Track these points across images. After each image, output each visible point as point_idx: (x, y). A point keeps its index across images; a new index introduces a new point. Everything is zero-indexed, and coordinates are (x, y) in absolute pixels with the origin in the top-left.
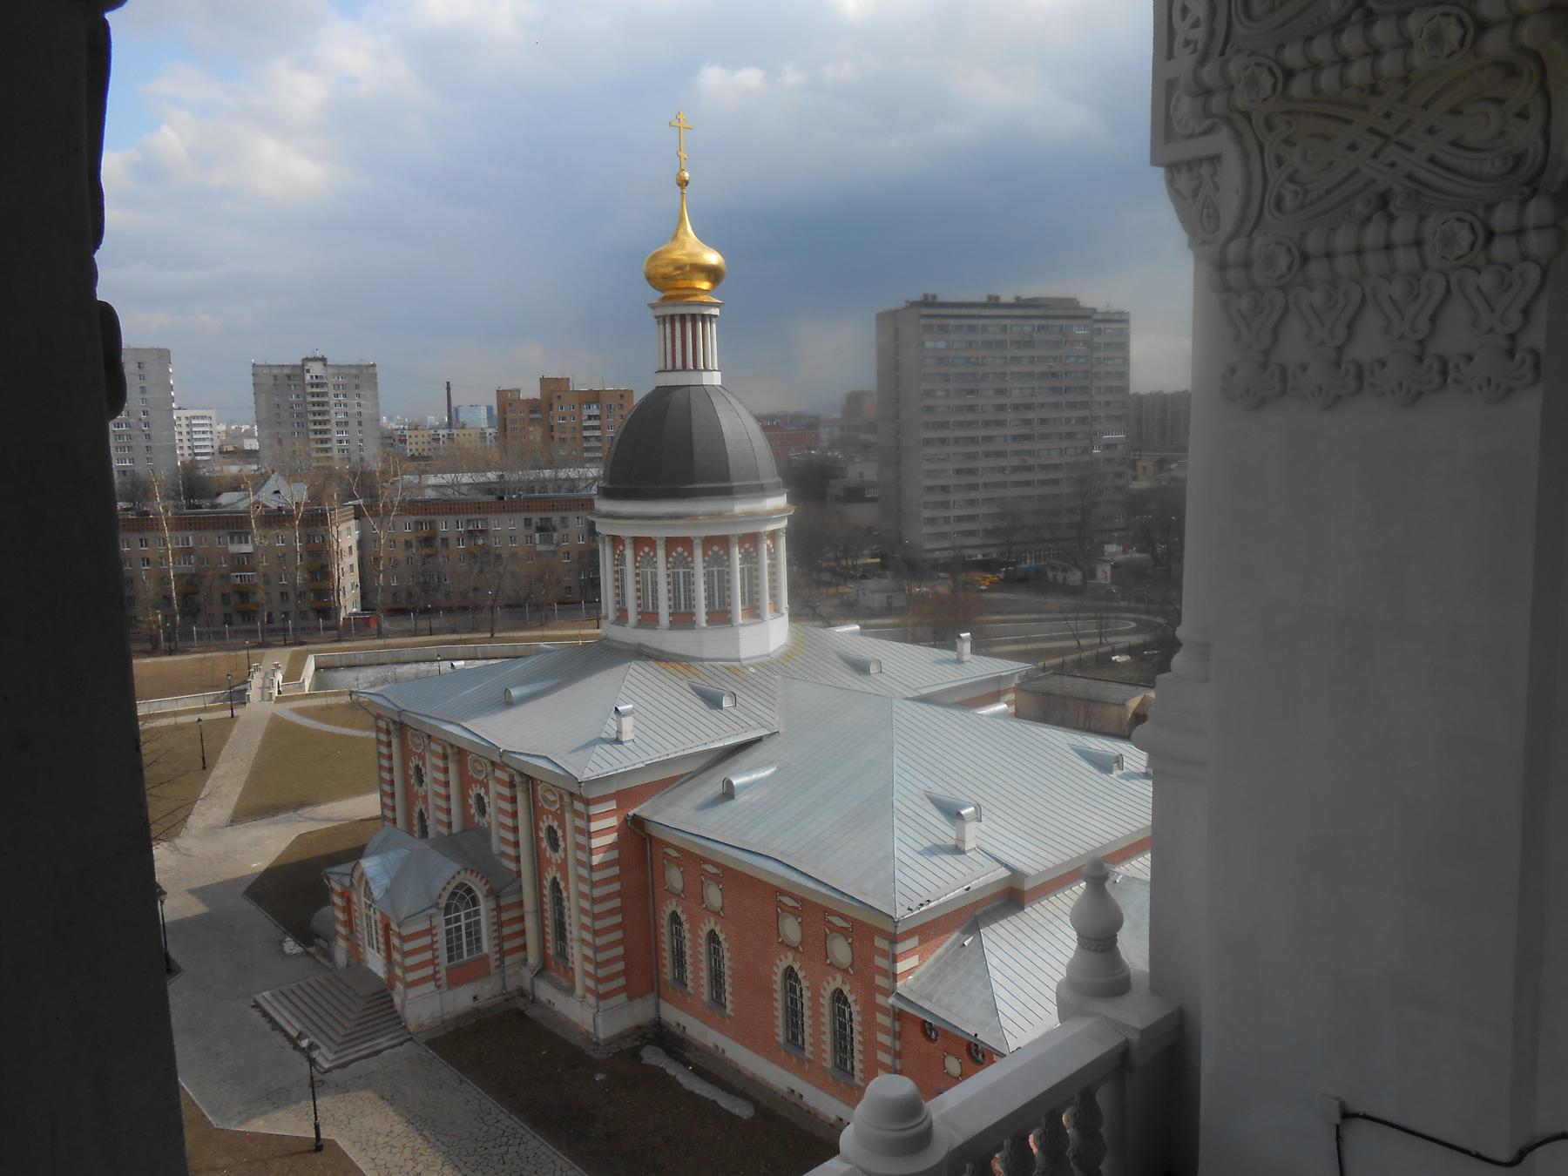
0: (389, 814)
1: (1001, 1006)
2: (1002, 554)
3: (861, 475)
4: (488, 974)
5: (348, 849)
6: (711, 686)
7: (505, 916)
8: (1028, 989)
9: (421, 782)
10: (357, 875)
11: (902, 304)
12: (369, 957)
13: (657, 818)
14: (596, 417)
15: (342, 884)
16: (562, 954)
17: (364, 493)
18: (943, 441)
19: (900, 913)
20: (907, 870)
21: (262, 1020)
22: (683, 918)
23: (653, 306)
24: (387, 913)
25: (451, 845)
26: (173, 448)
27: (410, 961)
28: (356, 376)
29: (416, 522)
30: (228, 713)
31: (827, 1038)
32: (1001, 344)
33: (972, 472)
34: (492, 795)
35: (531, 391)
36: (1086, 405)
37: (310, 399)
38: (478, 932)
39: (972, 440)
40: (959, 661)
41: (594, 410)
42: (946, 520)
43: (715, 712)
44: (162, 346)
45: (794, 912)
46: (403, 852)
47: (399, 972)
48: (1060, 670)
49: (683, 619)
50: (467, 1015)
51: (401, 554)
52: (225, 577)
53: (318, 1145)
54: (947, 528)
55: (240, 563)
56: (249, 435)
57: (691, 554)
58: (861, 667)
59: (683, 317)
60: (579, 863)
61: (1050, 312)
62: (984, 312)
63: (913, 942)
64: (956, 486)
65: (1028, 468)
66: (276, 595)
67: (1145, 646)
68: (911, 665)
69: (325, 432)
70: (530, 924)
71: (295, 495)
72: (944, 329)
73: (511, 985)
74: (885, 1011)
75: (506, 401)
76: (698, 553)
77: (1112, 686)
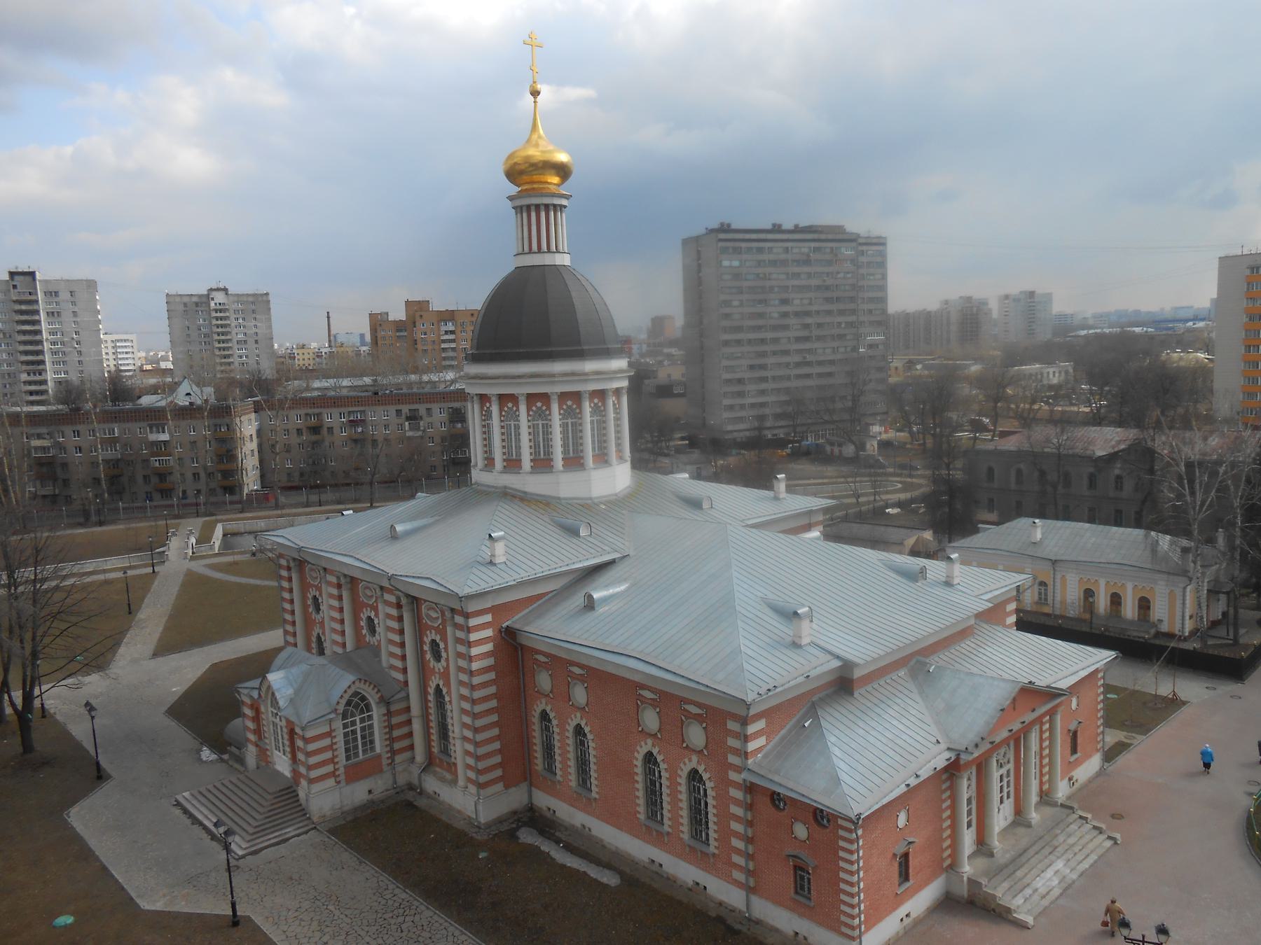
0: (291, 639)
1: (843, 776)
2: (788, 434)
3: (669, 376)
4: (381, 771)
5: (260, 664)
6: (569, 521)
7: (395, 720)
8: (865, 761)
9: (318, 609)
10: (264, 689)
11: (704, 231)
12: (276, 759)
13: (526, 629)
14: (452, 332)
15: (251, 697)
16: (445, 751)
17: (263, 391)
18: (739, 342)
19: (750, 698)
20: (753, 662)
21: (184, 818)
22: (552, 715)
23: (511, 198)
24: (293, 719)
25: (346, 661)
26: (101, 362)
27: (313, 760)
28: (253, 303)
29: (307, 414)
30: (150, 570)
31: (685, 813)
32: (784, 263)
33: (763, 367)
34: (381, 616)
35: (398, 313)
36: (853, 312)
37: (214, 322)
38: (372, 734)
39: (763, 341)
40: (776, 498)
41: (450, 327)
42: (742, 407)
43: (574, 540)
44: (90, 278)
45: (653, 704)
46: (304, 667)
47: (303, 770)
48: (845, 519)
49: (542, 463)
50: (363, 807)
51: (294, 440)
52: (146, 461)
53: (235, 921)
54: (743, 414)
55: (160, 448)
56: (165, 359)
57: (549, 408)
58: (695, 504)
59: (538, 207)
60: (460, 669)
61: (823, 237)
62: (770, 236)
63: (761, 724)
64: (749, 379)
65: (809, 364)
66: (189, 476)
67: (912, 501)
68: (735, 503)
69: (228, 349)
70: (417, 726)
71: (204, 395)
72: (737, 251)
73: (402, 780)
74: (736, 785)
75: (377, 322)
76: (555, 407)
77: (891, 529)
